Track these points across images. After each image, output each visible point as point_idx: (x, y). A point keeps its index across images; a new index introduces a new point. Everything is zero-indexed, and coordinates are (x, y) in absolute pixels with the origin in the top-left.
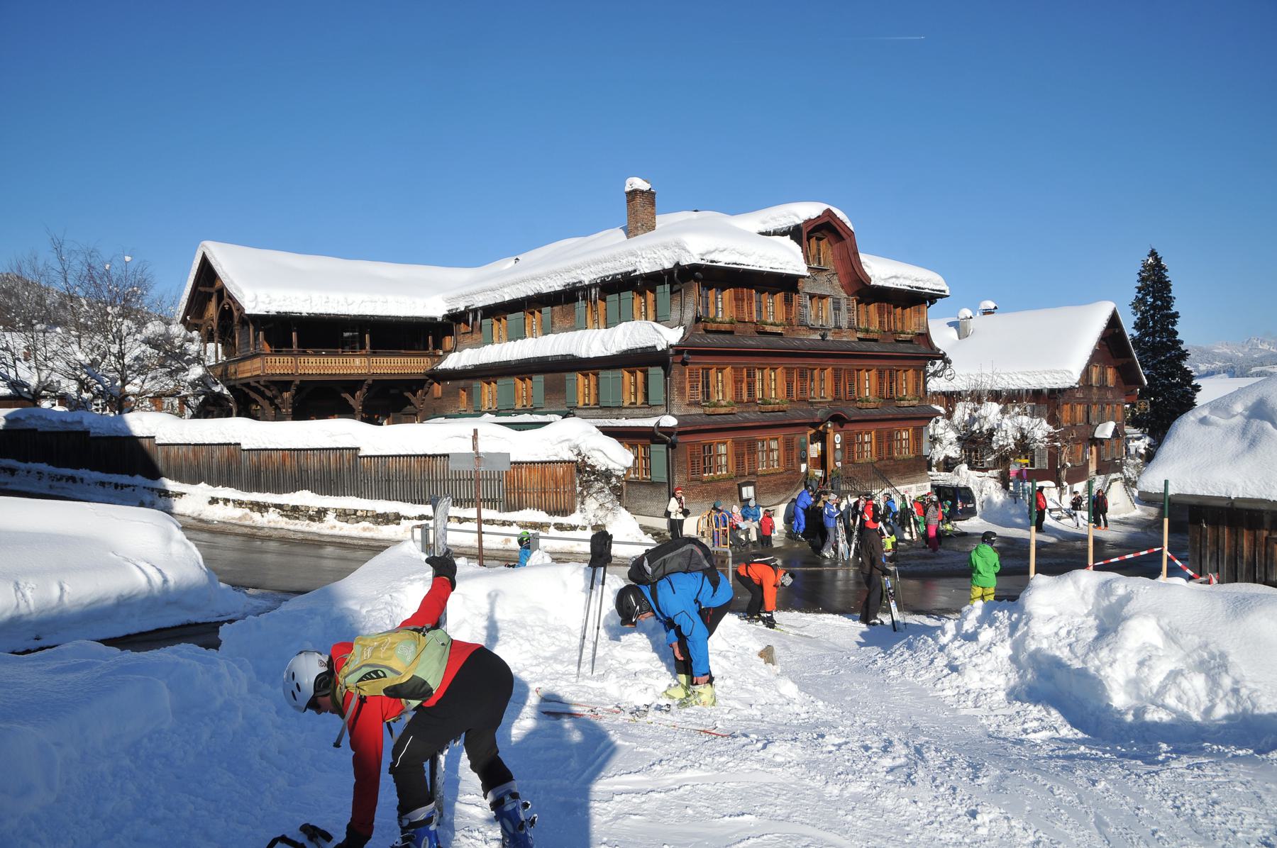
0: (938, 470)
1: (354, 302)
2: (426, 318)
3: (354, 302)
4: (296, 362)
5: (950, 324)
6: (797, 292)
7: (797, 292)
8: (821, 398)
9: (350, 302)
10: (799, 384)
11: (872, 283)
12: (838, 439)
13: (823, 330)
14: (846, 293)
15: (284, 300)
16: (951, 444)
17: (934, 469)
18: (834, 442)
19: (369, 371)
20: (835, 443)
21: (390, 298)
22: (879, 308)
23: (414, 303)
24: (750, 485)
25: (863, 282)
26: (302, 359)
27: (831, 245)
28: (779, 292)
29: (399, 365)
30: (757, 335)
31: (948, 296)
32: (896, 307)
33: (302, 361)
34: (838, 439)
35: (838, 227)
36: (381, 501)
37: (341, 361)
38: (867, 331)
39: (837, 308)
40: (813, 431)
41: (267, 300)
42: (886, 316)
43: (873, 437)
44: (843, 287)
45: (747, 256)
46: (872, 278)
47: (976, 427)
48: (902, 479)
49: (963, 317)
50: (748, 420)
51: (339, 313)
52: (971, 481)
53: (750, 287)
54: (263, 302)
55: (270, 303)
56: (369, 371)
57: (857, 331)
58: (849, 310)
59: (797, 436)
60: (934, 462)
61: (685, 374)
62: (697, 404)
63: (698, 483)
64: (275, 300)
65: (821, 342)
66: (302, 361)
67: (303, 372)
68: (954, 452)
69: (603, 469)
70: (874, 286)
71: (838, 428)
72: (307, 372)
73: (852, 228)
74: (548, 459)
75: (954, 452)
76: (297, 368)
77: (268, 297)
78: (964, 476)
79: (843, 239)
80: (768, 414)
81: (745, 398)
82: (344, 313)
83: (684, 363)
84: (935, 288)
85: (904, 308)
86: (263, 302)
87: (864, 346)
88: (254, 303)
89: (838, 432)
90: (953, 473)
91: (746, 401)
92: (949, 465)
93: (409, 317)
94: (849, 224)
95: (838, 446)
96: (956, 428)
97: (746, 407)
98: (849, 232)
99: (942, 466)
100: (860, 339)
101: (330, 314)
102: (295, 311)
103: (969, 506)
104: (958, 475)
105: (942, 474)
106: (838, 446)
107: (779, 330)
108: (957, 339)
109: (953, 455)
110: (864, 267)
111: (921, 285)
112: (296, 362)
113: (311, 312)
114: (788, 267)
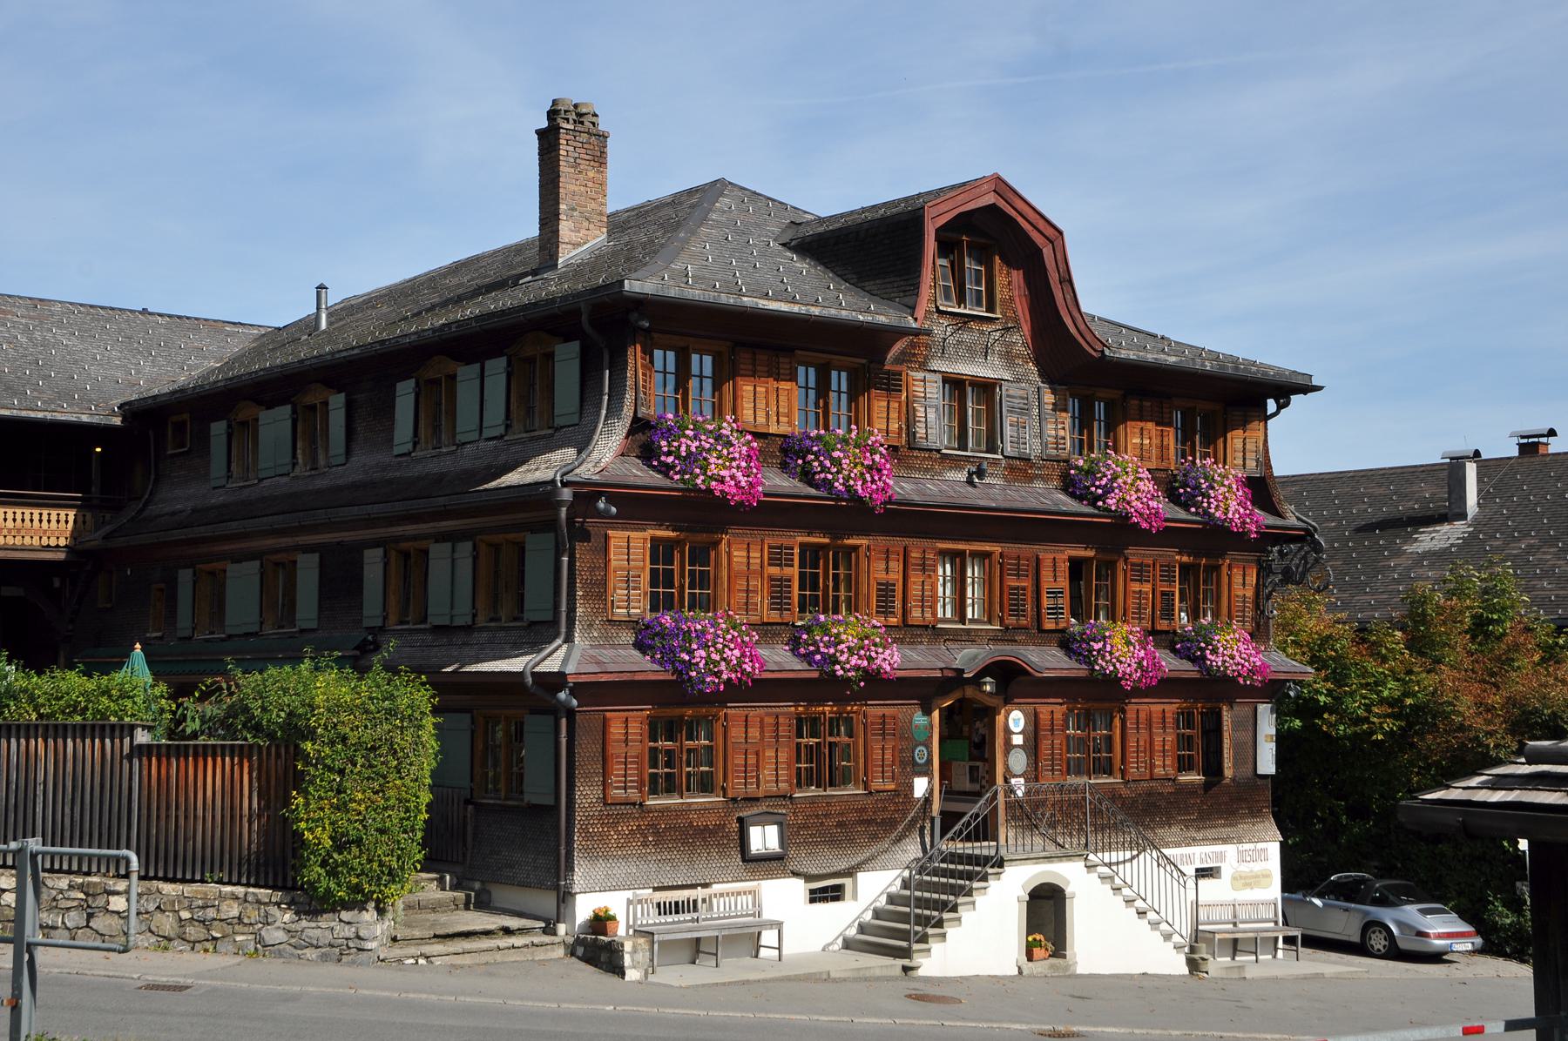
34: (1016, 721)
95: (1018, 740)
106: (1018, 740)
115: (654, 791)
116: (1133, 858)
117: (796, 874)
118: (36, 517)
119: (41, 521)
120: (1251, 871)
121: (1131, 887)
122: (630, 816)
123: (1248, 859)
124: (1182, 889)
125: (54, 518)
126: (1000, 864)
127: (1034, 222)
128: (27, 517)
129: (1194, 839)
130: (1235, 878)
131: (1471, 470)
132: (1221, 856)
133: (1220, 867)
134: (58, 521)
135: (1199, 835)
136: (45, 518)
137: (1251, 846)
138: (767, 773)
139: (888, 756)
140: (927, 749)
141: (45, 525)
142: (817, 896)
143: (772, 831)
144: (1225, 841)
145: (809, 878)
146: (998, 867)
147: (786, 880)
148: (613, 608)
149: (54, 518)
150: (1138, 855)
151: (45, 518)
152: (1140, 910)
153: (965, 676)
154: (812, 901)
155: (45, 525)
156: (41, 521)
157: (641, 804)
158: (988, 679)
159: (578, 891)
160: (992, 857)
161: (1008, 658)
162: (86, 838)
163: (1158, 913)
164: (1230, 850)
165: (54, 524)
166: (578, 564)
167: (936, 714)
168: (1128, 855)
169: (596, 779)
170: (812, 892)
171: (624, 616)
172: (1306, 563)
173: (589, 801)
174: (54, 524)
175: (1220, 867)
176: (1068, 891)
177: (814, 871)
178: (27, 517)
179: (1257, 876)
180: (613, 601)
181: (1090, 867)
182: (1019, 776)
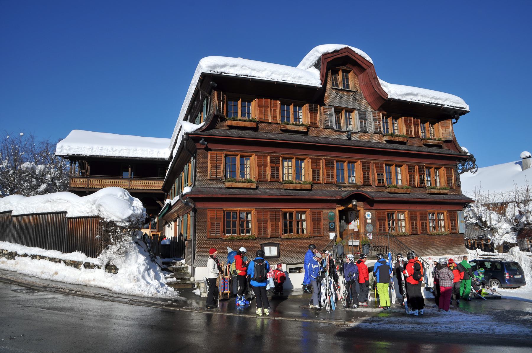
0: (498, 252)
1: (116, 150)
2: (159, 159)
3: (116, 150)
4: (88, 182)
5: (516, 163)
6: (322, 104)
7: (322, 104)
8: (349, 183)
9: (114, 149)
10: (325, 171)
11: (389, 97)
12: (368, 215)
13: (349, 134)
14: (373, 108)
15: (78, 148)
16: (507, 233)
17: (496, 251)
18: (365, 217)
19: (129, 187)
20: (366, 219)
21: (139, 148)
22: (406, 121)
23: (152, 151)
24: (275, 246)
25: (382, 98)
26: (92, 180)
27: (357, 76)
28: (305, 104)
29: (147, 184)
30: (281, 132)
31: (468, 112)
32: (424, 122)
33: (92, 181)
34: (368, 215)
35: (358, 61)
36: (49, 250)
37: (114, 182)
38: (392, 135)
39: (363, 117)
40: (342, 208)
41: (68, 148)
42: (413, 126)
43: (406, 216)
44: (369, 104)
45: (259, 71)
46: (389, 94)
47: (524, 219)
48: (438, 250)
49: (524, 157)
50: (266, 193)
51: (108, 155)
52: (523, 259)
53: (275, 98)
54: (66, 149)
55: (69, 150)
56: (129, 187)
57: (384, 136)
58: (375, 121)
59: (324, 211)
60: (495, 246)
61: (207, 157)
62: (218, 180)
63: (219, 241)
64: (72, 148)
65: (348, 141)
66: (92, 181)
67: (91, 187)
68: (511, 238)
69: (108, 221)
70: (390, 99)
71: (369, 207)
72: (94, 187)
73: (371, 61)
74: (88, 215)
75: (511, 238)
76: (88, 184)
77: (69, 147)
78: (517, 255)
79: (365, 70)
80: (290, 191)
81: (268, 178)
82: (110, 155)
83: (208, 149)
84: (455, 106)
85: (432, 123)
86: (66, 149)
87: (389, 146)
88: (60, 150)
89: (369, 210)
90: (508, 254)
91: (269, 180)
92: (506, 247)
93: (148, 158)
94: (368, 58)
95: (369, 221)
96: (509, 222)
97: (270, 185)
98: (368, 64)
99: (502, 249)
100: (388, 142)
101: (103, 156)
102: (83, 154)
103: (516, 277)
104: (512, 255)
105: (500, 254)
106: (369, 221)
107: (446, 191)
108: (522, 170)
109: (511, 241)
110: (382, 87)
111: (440, 102)
112: (88, 182)
113: (91, 155)
114: (301, 81)
118: (153, 183)
119: (154, 184)
123: (457, 260)
125: (157, 183)
127: (363, 61)
128: (151, 183)
131: (520, 276)
134: (158, 184)
136: (155, 183)
137: (458, 256)
140: (335, 224)
141: (155, 185)
149: (157, 183)
151: (155, 183)
155: (155, 185)
156: (154, 184)
161: (360, 193)
162: (80, 250)
165: (157, 184)
171: (215, 178)
172: (469, 165)
173: (202, 237)
174: (157, 184)
178: (151, 183)
182: (370, 233)
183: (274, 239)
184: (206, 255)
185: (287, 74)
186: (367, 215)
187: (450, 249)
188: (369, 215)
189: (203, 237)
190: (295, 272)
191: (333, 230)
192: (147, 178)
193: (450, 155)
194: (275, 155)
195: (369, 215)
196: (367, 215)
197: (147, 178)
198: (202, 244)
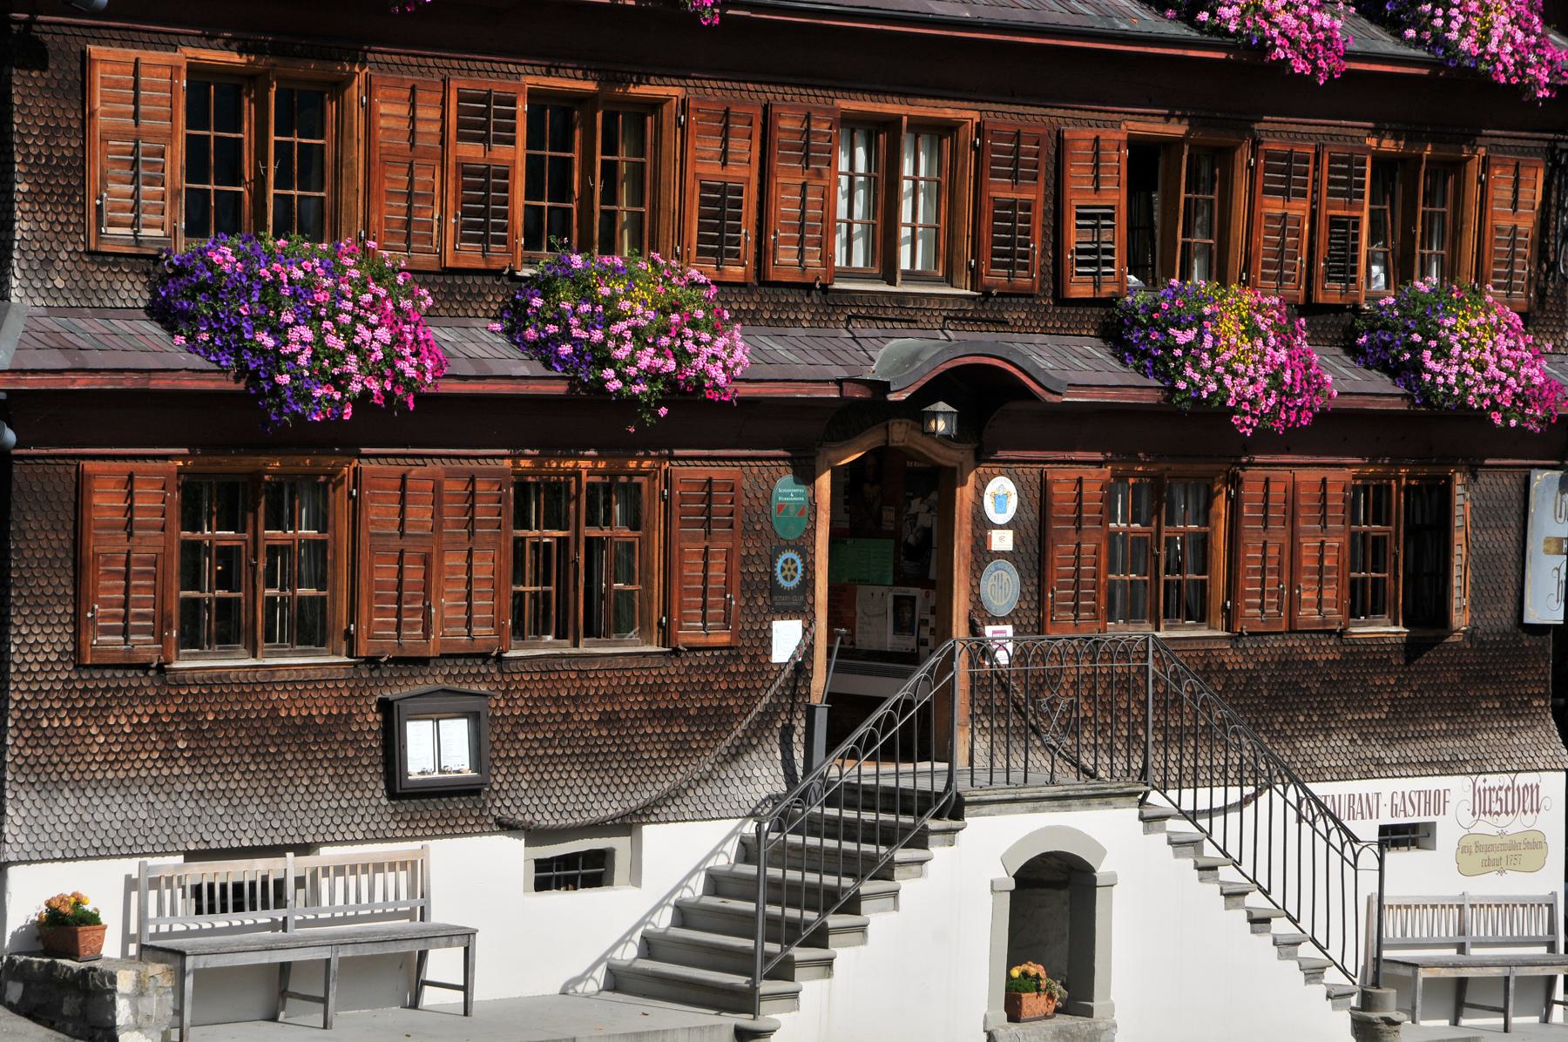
34: (1000, 500)
95: (1002, 541)
106: (1002, 541)
115: (191, 640)
116: (1244, 802)
117: (506, 827)
120: (1502, 834)
121: (1237, 864)
122: (137, 694)
124: (1349, 870)
126: (955, 809)
129: (1380, 763)
130: (1463, 849)
132: (1437, 801)
133: (1434, 824)
135: (1393, 755)
137: (1505, 780)
138: (448, 604)
139: (717, 572)
140: (803, 557)
142: (550, 876)
143: (456, 733)
144: (1448, 767)
145: (534, 835)
146: (951, 817)
147: (476, 839)
148: (99, 224)
150: (1255, 796)
152: (1256, 915)
153: (892, 397)
154: (541, 885)
157: (161, 669)
158: (942, 406)
159: (13, 857)
160: (939, 795)
163: (1295, 922)
164: (1458, 787)
166: (17, 120)
167: (824, 481)
168: (1234, 795)
169: (59, 610)
170: (541, 865)
175: (1434, 824)
176: (1102, 870)
177: (546, 820)
179: (1514, 846)
180: (99, 208)
181: (1151, 821)
183: (460, 662)
184: (66, 777)
185: (493, 332)
186: (995, 496)
187: (1462, 735)
188: (1007, 496)
189: (53, 658)
190: (570, 883)
191: (797, 606)
192: (1146, 114)
193: (1126, 109)
194: (648, 585)
195: (1007, 496)
196: (995, 496)
197: (1146, 114)
198: (47, 705)
